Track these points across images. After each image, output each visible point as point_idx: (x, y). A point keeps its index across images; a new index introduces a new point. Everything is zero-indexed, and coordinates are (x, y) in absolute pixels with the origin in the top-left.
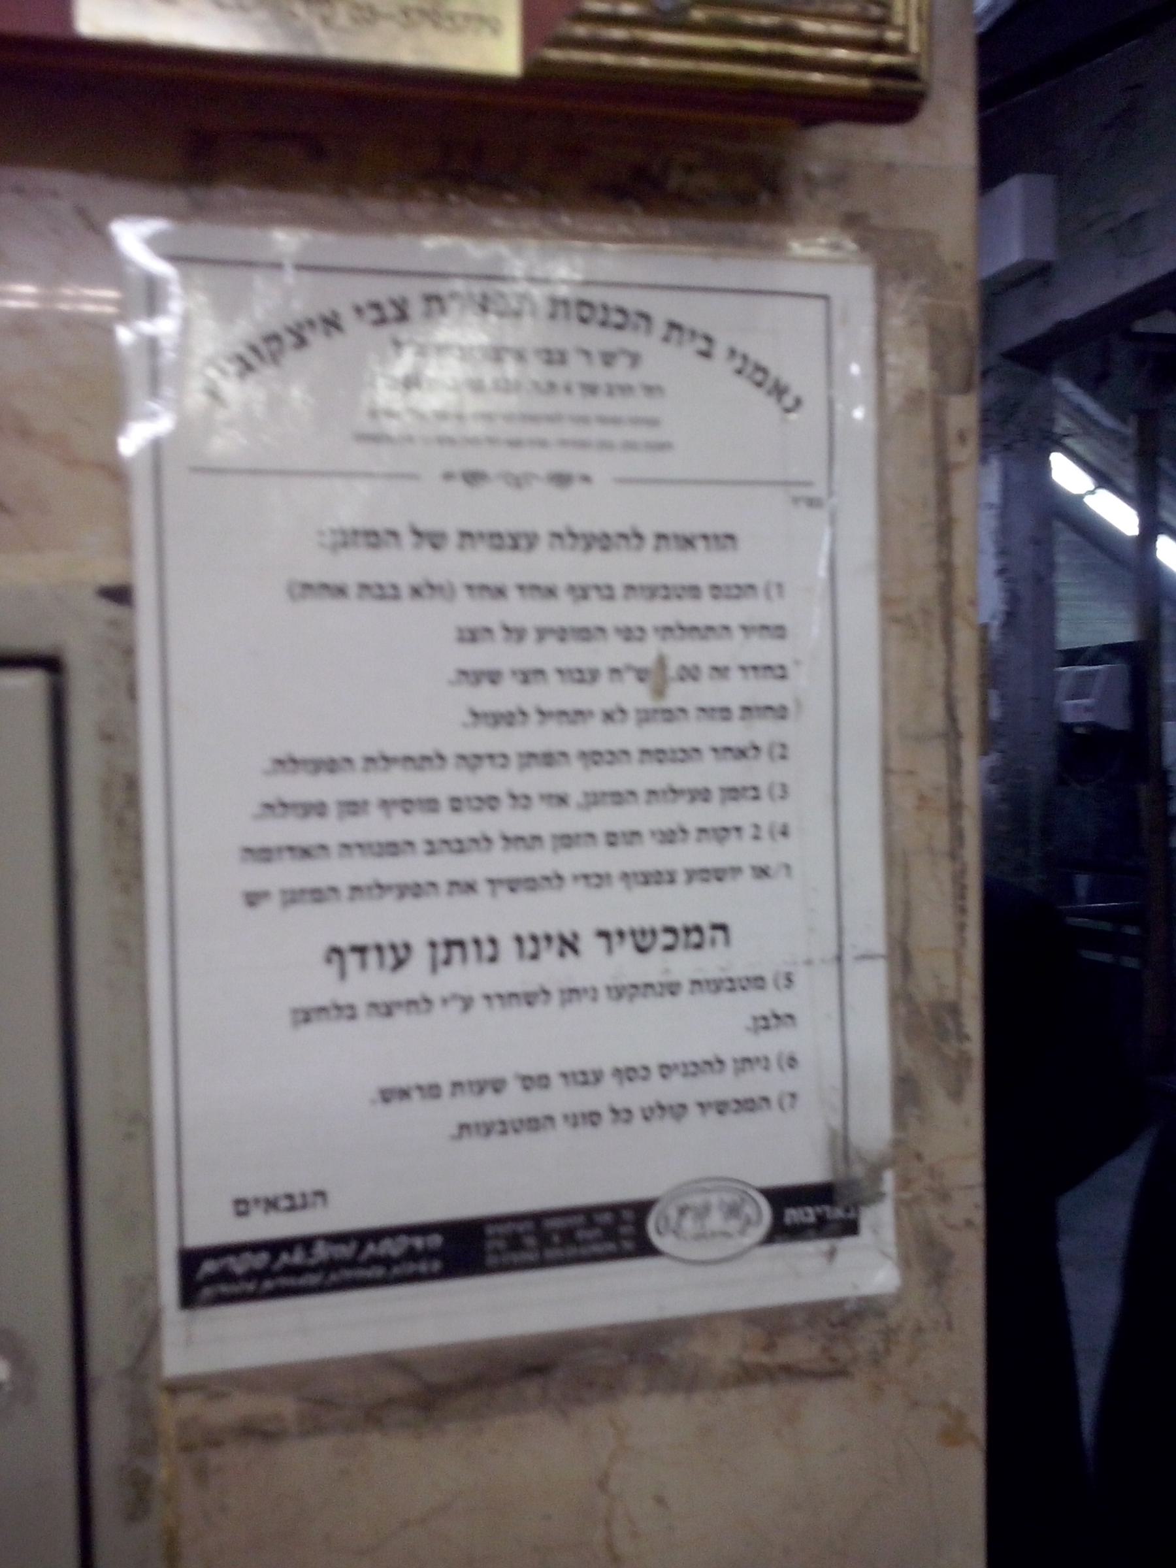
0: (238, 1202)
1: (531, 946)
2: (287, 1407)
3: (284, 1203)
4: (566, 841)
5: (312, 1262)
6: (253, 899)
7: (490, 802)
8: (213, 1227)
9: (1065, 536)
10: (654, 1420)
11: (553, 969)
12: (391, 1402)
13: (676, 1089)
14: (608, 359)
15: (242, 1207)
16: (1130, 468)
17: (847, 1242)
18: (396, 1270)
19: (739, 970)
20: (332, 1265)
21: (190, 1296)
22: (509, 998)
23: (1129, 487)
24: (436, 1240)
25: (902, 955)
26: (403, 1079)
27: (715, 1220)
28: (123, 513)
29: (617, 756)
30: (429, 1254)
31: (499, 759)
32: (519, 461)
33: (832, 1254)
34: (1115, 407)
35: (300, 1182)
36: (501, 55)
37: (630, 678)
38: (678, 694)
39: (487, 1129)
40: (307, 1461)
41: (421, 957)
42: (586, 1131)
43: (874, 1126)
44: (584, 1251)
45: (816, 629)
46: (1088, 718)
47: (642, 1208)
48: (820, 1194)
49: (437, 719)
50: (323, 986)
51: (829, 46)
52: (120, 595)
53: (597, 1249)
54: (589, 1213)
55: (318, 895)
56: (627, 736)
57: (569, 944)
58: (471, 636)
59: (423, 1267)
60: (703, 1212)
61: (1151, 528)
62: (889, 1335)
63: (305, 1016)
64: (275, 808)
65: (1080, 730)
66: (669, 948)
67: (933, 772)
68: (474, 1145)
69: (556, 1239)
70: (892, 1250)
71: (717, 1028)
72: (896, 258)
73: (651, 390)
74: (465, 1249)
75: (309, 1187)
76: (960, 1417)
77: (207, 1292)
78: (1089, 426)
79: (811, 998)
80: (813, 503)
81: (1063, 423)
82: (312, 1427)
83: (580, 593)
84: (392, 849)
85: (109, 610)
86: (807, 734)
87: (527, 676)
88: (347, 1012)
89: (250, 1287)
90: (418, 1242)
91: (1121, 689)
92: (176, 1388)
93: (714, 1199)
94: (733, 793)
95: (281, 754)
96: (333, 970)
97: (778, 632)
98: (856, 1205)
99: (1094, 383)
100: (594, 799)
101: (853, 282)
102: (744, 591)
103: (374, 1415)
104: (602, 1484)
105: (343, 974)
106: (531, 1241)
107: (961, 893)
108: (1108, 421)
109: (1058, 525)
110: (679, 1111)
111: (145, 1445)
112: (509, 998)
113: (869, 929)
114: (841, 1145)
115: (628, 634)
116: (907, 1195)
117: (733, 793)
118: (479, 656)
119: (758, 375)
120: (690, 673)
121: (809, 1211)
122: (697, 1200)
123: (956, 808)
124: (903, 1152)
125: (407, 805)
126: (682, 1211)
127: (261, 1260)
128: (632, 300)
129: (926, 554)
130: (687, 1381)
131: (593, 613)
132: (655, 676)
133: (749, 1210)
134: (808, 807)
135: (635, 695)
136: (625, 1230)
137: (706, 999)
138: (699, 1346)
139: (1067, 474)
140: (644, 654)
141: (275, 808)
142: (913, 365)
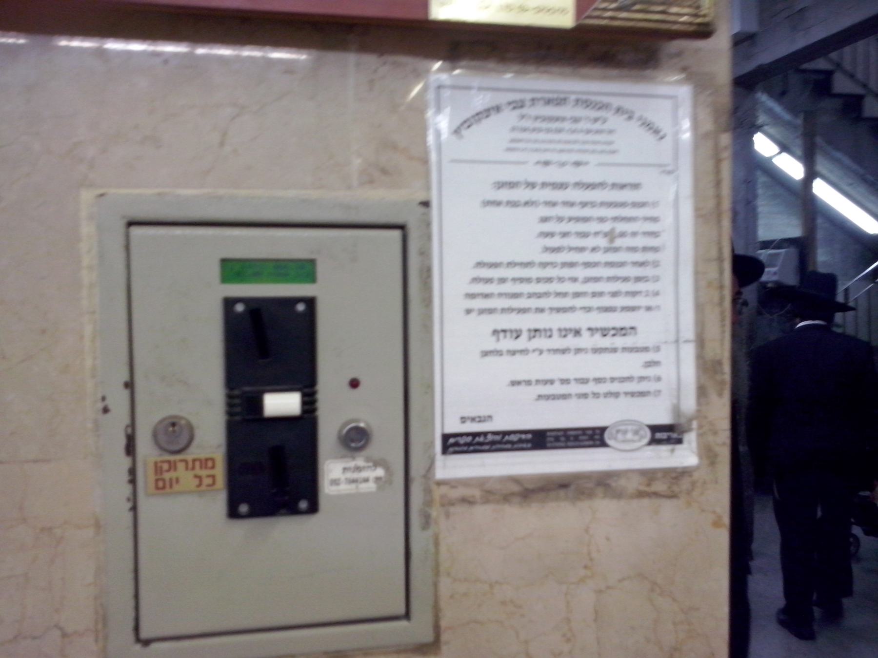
0: (462, 418)
1: (564, 332)
2: (477, 493)
3: (477, 419)
4: (577, 295)
5: (487, 441)
6: (469, 311)
7: (549, 280)
8: (455, 426)
9: (762, 179)
10: (605, 508)
11: (571, 341)
12: (513, 494)
13: (615, 387)
14: (596, 120)
15: (463, 420)
16: (799, 142)
17: (678, 447)
18: (516, 446)
19: (640, 344)
20: (493, 443)
21: (445, 450)
22: (556, 351)
23: (799, 152)
24: (529, 436)
25: (700, 342)
26: (519, 377)
27: (629, 436)
28: (427, 174)
29: (595, 265)
30: (527, 441)
31: (553, 264)
32: (564, 157)
33: (673, 451)
34: (792, 109)
35: (484, 413)
36: (566, 20)
37: (601, 236)
38: (619, 242)
39: (548, 397)
40: (483, 513)
41: (525, 336)
42: (582, 401)
43: (689, 404)
44: (582, 444)
45: (668, 220)
46: (775, 278)
47: (603, 430)
48: (669, 428)
49: (531, 249)
50: (491, 344)
51: (681, 15)
52: (426, 204)
53: (587, 443)
54: (584, 430)
55: (491, 311)
56: (598, 257)
57: (577, 332)
58: (545, 220)
59: (524, 445)
60: (625, 432)
62: (693, 484)
63: (485, 354)
64: (476, 280)
65: (770, 285)
66: (614, 335)
67: (713, 274)
68: (543, 403)
69: (572, 438)
70: (695, 450)
71: (631, 365)
72: (699, 82)
73: (611, 132)
74: (539, 440)
75: (487, 413)
76: (720, 517)
77: (451, 449)
78: (776, 119)
79: (666, 355)
80: (670, 172)
81: (762, 119)
82: (486, 501)
83: (584, 205)
84: (516, 296)
85: (422, 209)
86: (666, 257)
87: (565, 235)
88: (499, 353)
89: (465, 448)
90: (523, 436)
92: (440, 483)
93: (630, 427)
94: (638, 279)
95: (479, 260)
96: (494, 338)
97: (655, 220)
98: (683, 432)
99: (781, 96)
100: (587, 280)
101: (684, 92)
102: (642, 205)
103: (506, 498)
104: (587, 530)
105: (498, 340)
106: (563, 439)
107: (723, 320)
108: (787, 116)
109: (759, 173)
110: (616, 395)
111: (429, 503)
112: (556, 351)
113: (689, 331)
114: (676, 410)
115: (602, 220)
116: (701, 431)
117: (638, 279)
118: (547, 227)
119: (648, 125)
120: (623, 235)
121: (665, 434)
122: (623, 428)
123: (721, 287)
124: (699, 415)
125: (522, 280)
126: (618, 431)
127: (469, 439)
128: (605, 99)
129: (711, 192)
130: (618, 495)
131: (587, 212)
132: (611, 235)
133: (642, 432)
134: (666, 285)
135: (602, 242)
136: (597, 437)
137: (627, 355)
138: (623, 482)
139: (763, 145)
140: (606, 227)
141: (476, 280)
142: (708, 126)
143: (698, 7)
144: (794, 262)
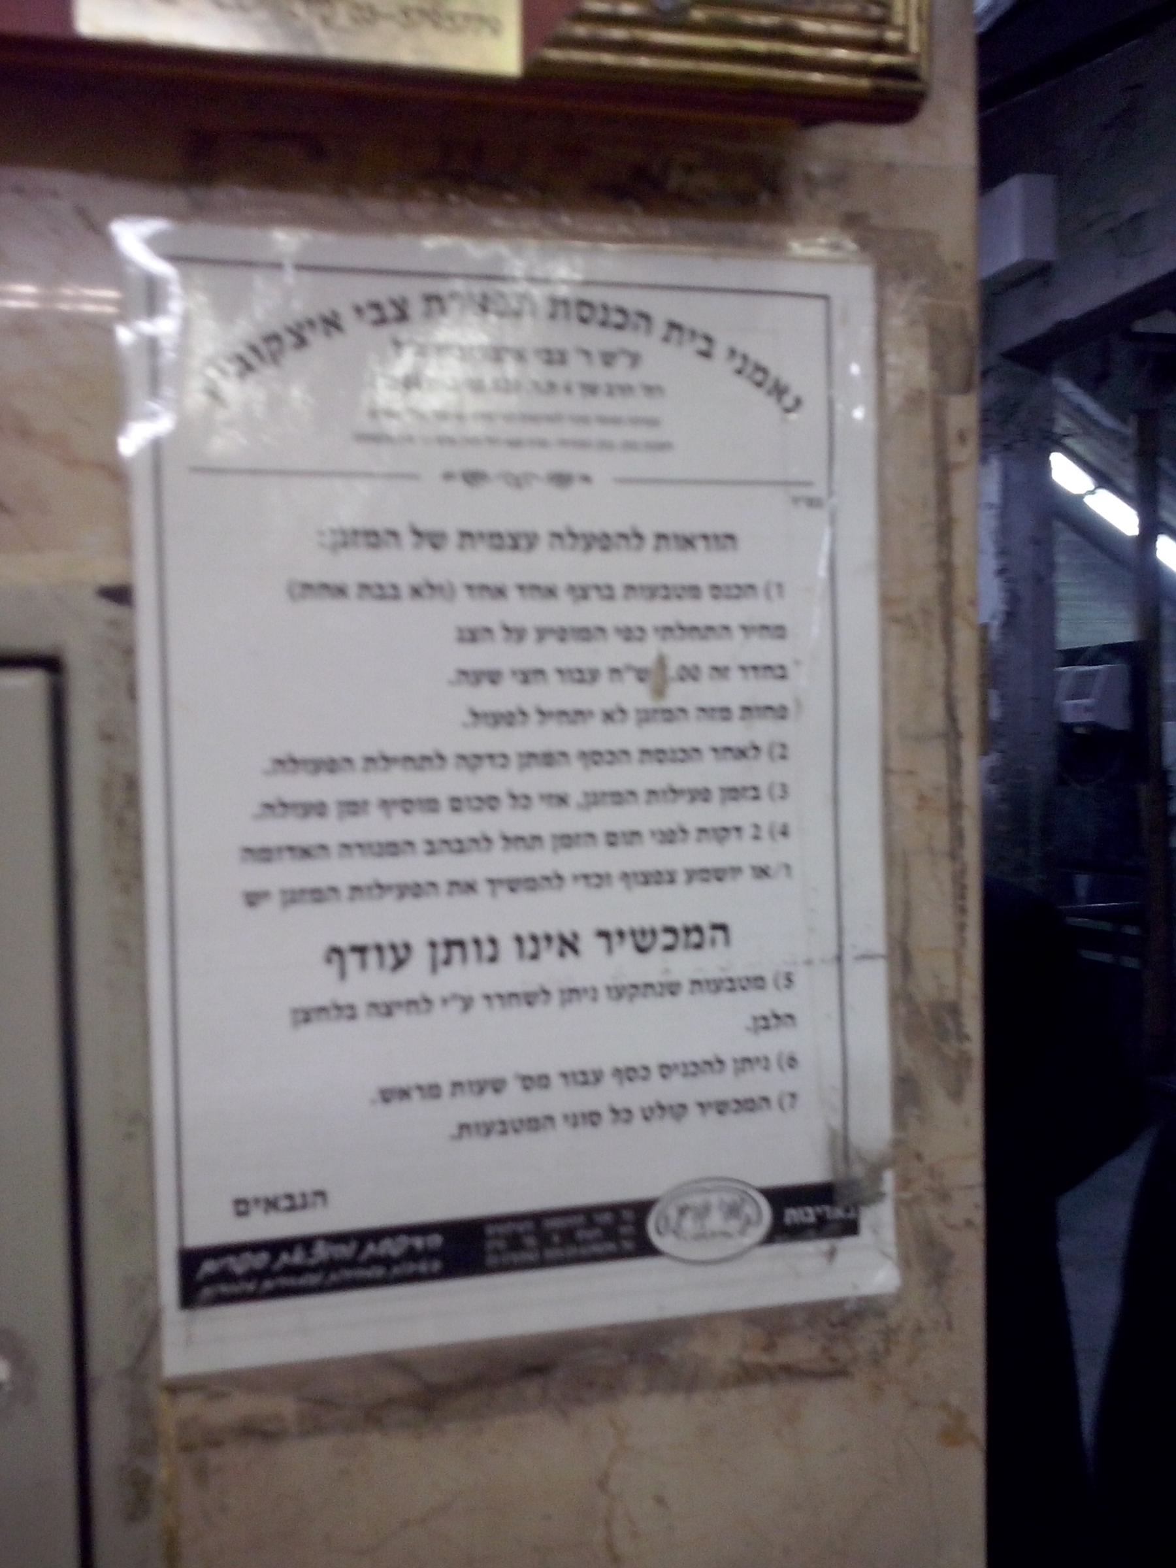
0: (238, 1202)
1: (531, 946)
2: (287, 1407)
3: (284, 1203)
4: (566, 841)
5: (312, 1262)
6: (253, 899)
7: (490, 802)
8: (213, 1227)
9: (1065, 536)
10: (654, 1420)
11: (553, 969)
12: (391, 1402)
13: (676, 1089)
14: (608, 359)
15: (242, 1207)
16: (1130, 468)
17: (847, 1242)
18: (396, 1270)
19: (739, 970)
20: (332, 1265)
21: (190, 1296)
22: (509, 998)
23: (1129, 487)
24: (436, 1240)
25: (902, 955)
26: (403, 1079)
27: (715, 1220)
28: (123, 513)
29: (617, 756)
30: (429, 1254)
31: (499, 759)
32: (519, 461)
33: (832, 1254)
34: (1115, 407)
35: (300, 1182)
36: (501, 55)
37: (630, 678)
38: (678, 694)
39: (487, 1129)
40: (307, 1461)
41: (421, 957)
42: (586, 1131)
43: (874, 1126)
44: (584, 1251)
45: (816, 629)
46: (1088, 718)
47: (642, 1208)
48: (820, 1194)
49: (437, 719)
50: (323, 986)
51: (829, 46)
52: (120, 595)
53: (597, 1249)
54: (589, 1213)
55: (318, 895)
56: (627, 736)
57: (569, 944)
58: (471, 636)
59: (423, 1267)
60: (703, 1212)
62: (889, 1335)
63: (305, 1016)
64: (275, 808)
65: (1080, 730)
66: (669, 948)
67: (933, 772)
68: (474, 1145)
69: (556, 1239)
70: (892, 1250)
71: (717, 1028)
72: (896, 258)
73: (651, 390)
74: (465, 1249)
75: (309, 1187)
76: (960, 1417)
77: (207, 1292)
78: (1089, 426)
79: (811, 998)
80: (813, 503)
81: (1063, 423)
82: (312, 1427)
83: (580, 593)
84: (392, 849)
85: (109, 610)
86: (807, 734)
87: (527, 676)
88: (347, 1012)
89: (250, 1287)
90: (418, 1242)
92: (176, 1388)
93: (714, 1199)
94: (733, 793)
95: (281, 754)
96: (333, 970)
97: (778, 632)
98: (856, 1205)
99: (1094, 383)
100: (594, 799)
101: (853, 282)
102: (744, 591)
103: (374, 1415)
104: (602, 1484)
105: (343, 974)
106: (531, 1241)
107: (961, 893)
108: (1108, 421)
109: (1058, 525)
110: (679, 1111)
111: (145, 1445)
112: (509, 998)
113: (869, 929)
114: (841, 1145)
115: (628, 634)
116: (907, 1195)
117: (733, 793)
118: (479, 656)
119: (758, 375)
120: (690, 673)
121: (809, 1211)
122: (697, 1200)
123: (956, 808)
124: (903, 1152)
125: (407, 805)
126: (682, 1211)
127: (261, 1260)
128: (632, 300)
129: (926, 554)
130: (687, 1381)
131: (593, 613)
132: (655, 676)
133: (749, 1210)
134: (808, 807)
135: (635, 695)
136: (625, 1230)
137: (706, 999)
138: (699, 1346)
139: (1067, 474)
140: (644, 654)
141: (275, 808)
142: (913, 365)
143: (883, 22)
144: (1121, 689)
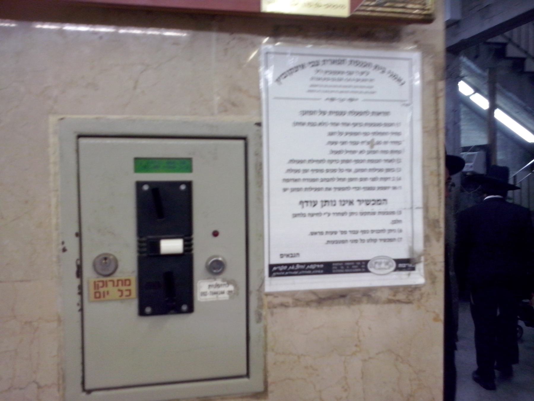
0: (281, 255)
1: (343, 203)
2: (290, 300)
3: (290, 256)
4: (351, 180)
5: (296, 269)
6: (285, 190)
7: (334, 171)
8: (276, 260)
9: (463, 109)
10: (368, 309)
11: (347, 208)
12: (312, 301)
13: (374, 236)
14: (362, 73)
15: (282, 256)
16: (486, 86)
17: (412, 272)
18: (314, 272)
19: (389, 210)
20: (300, 270)
21: (271, 274)
22: (338, 214)
23: (486, 93)
24: (322, 266)
25: (426, 208)
26: (316, 230)
27: (383, 266)
28: (260, 106)
29: (362, 161)
30: (320, 269)
31: (336, 161)
32: (343, 96)
33: (409, 275)
34: (482, 67)
35: (294, 251)
36: (344, 12)
37: (365, 144)
38: (376, 148)
39: (333, 242)
40: (293, 312)
41: (319, 205)
42: (354, 244)
43: (419, 246)
44: (354, 270)
45: (406, 134)
46: (471, 170)
47: (367, 262)
48: (407, 261)
49: (323, 152)
50: (298, 209)
51: (414, 9)
52: (259, 124)
53: (357, 270)
54: (355, 262)
55: (299, 190)
56: (364, 157)
57: (351, 203)
58: (331, 134)
59: (319, 271)
60: (380, 263)
61: (493, 106)
62: (422, 295)
63: (295, 216)
64: (290, 171)
65: (468, 174)
66: (373, 204)
67: (434, 167)
68: (330, 246)
69: (348, 267)
70: (423, 274)
71: (384, 222)
72: (425, 50)
73: (371, 80)
74: (328, 268)
75: (296, 252)
76: (438, 315)
77: (274, 274)
78: (472, 73)
79: (405, 217)
80: (407, 105)
81: (463, 72)
82: (296, 305)
83: (355, 125)
84: (314, 180)
85: (257, 128)
86: (405, 157)
87: (343, 143)
88: (303, 215)
89: (283, 273)
90: (318, 266)
91: (483, 160)
92: (267, 295)
93: (383, 261)
94: (388, 170)
95: (291, 158)
96: (300, 206)
97: (398, 134)
98: (415, 263)
99: (475, 58)
100: (357, 171)
101: (416, 56)
102: (391, 125)
103: (308, 304)
104: (357, 323)
105: (303, 207)
106: (342, 267)
107: (440, 195)
108: (479, 71)
109: (461, 105)
110: (375, 241)
111: (261, 306)
112: (338, 214)
113: (419, 202)
114: (411, 250)
115: (366, 134)
116: (426, 263)
117: (388, 170)
118: (333, 138)
119: (394, 76)
120: (379, 143)
121: (405, 265)
122: (379, 261)
123: (439, 175)
124: (425, 253)
125: (317, 171)
126: (376, 263)
127: (285, 267)
128: (368, 61)
129: (432, 117)
130: (376, 302)
131: (357, 129)
132: (371, 143)
133: (390, 264)
134: (405, 174)
135: (366, 148)
136: (363, 266)
137: (381, 216)
138: (379, 294)
139: (464, 88)
140: (369, 138)
141: (290, 171)
142: (431, 76)
143: (425, 4)
